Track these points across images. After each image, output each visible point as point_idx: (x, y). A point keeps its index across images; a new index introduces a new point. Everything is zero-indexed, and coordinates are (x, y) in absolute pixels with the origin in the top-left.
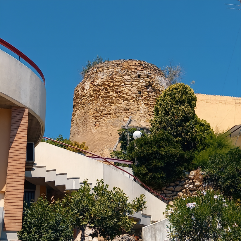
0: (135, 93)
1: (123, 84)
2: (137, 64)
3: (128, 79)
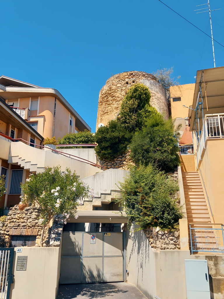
0: (123, 95)
1: (117, 90)
3: (119, 87)
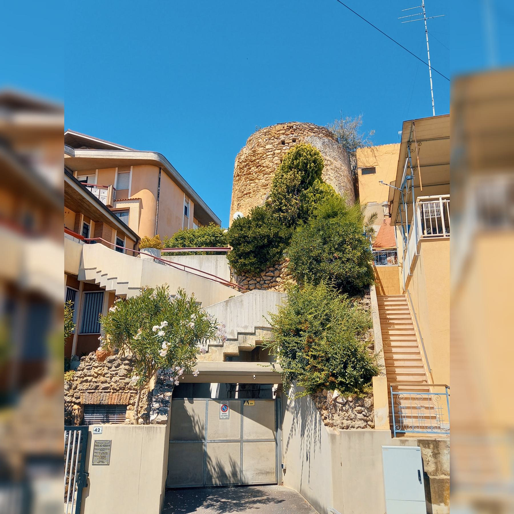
0: (276, 164)
1: (265, 155)
2: (286, 127)
3: (269, 149)
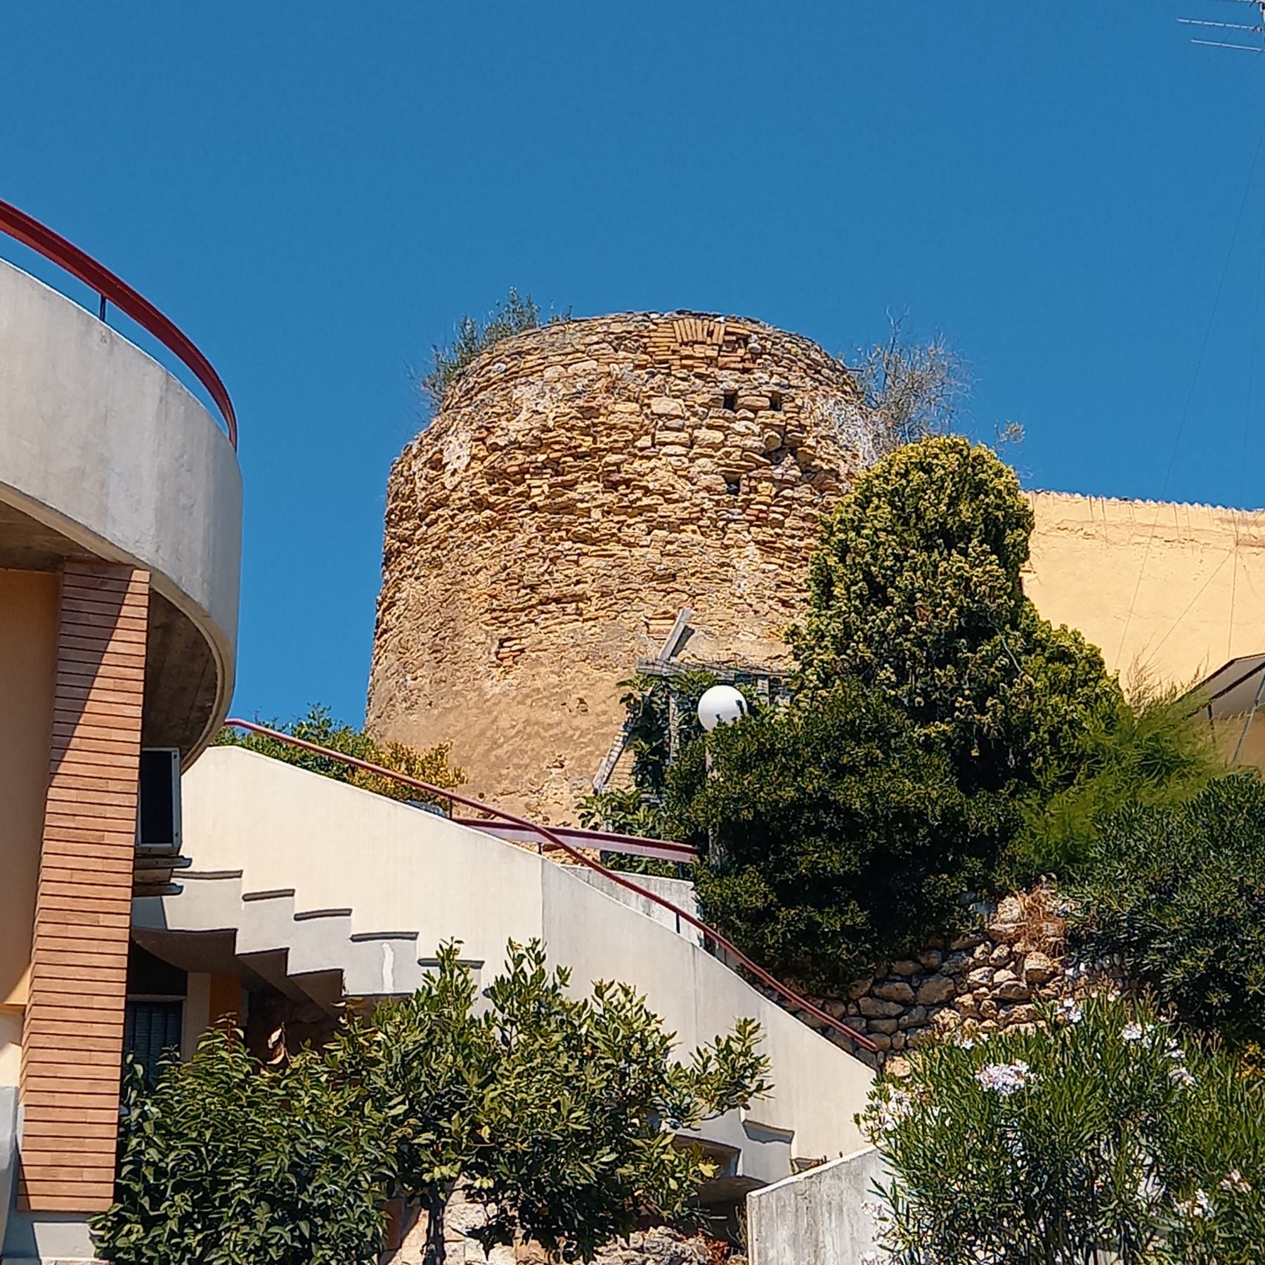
0: (708, 489)
2: (719, 337)
